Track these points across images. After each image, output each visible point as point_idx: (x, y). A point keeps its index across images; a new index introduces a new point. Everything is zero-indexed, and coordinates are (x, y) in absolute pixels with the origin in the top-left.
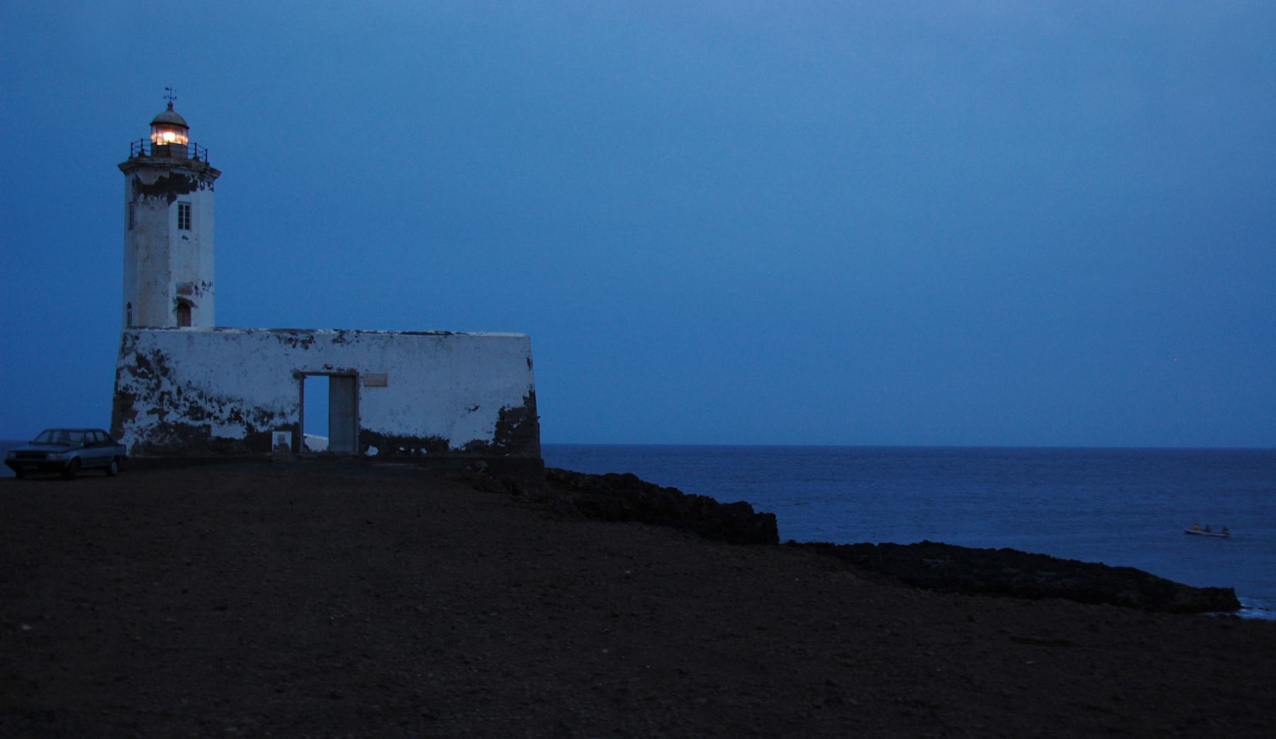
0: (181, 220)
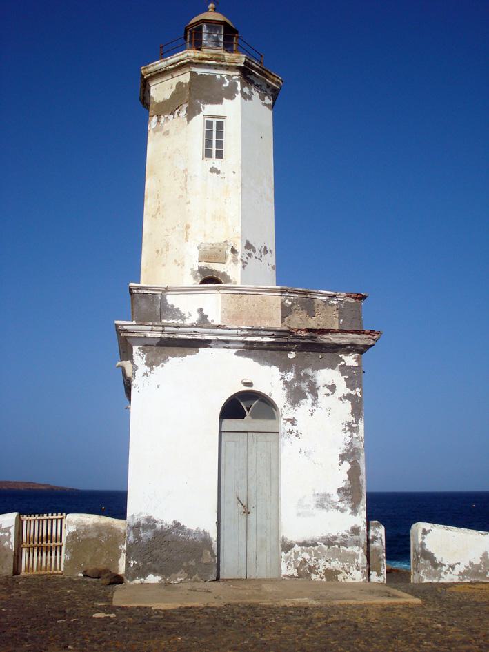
0: (208, 143)
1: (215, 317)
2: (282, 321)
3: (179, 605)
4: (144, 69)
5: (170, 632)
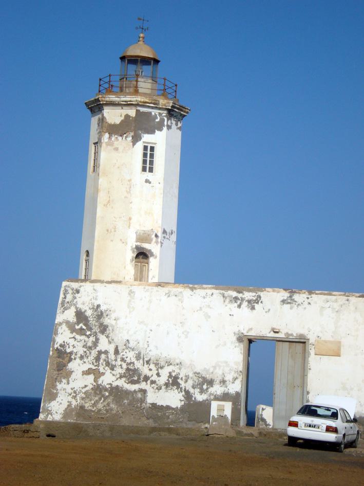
4: (102, 97)
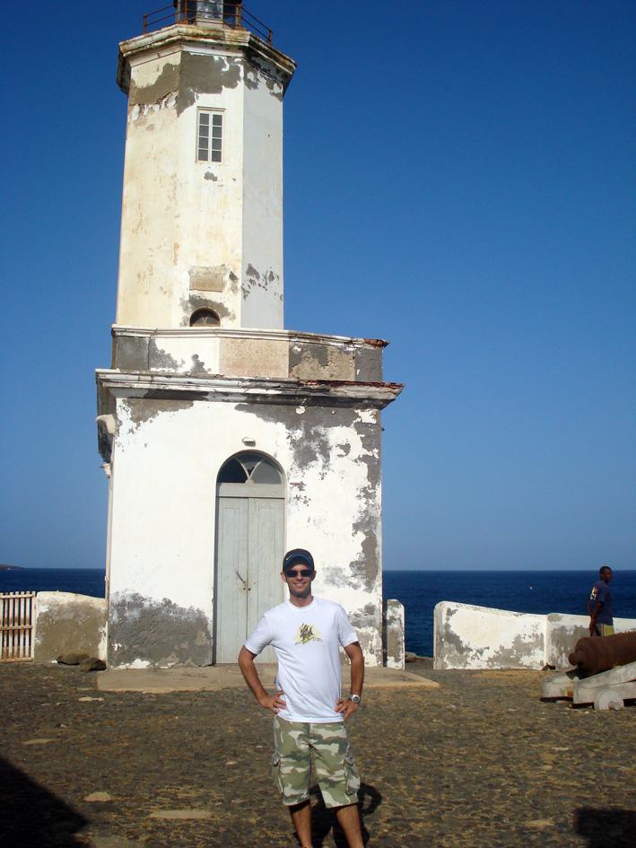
1: (213, 366)
2: (290, 371)
3: (172, 690)
5: (166, 712)
